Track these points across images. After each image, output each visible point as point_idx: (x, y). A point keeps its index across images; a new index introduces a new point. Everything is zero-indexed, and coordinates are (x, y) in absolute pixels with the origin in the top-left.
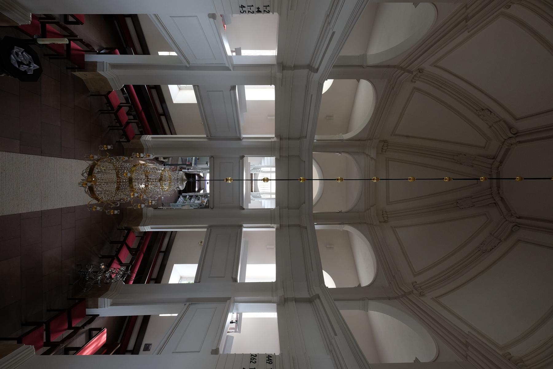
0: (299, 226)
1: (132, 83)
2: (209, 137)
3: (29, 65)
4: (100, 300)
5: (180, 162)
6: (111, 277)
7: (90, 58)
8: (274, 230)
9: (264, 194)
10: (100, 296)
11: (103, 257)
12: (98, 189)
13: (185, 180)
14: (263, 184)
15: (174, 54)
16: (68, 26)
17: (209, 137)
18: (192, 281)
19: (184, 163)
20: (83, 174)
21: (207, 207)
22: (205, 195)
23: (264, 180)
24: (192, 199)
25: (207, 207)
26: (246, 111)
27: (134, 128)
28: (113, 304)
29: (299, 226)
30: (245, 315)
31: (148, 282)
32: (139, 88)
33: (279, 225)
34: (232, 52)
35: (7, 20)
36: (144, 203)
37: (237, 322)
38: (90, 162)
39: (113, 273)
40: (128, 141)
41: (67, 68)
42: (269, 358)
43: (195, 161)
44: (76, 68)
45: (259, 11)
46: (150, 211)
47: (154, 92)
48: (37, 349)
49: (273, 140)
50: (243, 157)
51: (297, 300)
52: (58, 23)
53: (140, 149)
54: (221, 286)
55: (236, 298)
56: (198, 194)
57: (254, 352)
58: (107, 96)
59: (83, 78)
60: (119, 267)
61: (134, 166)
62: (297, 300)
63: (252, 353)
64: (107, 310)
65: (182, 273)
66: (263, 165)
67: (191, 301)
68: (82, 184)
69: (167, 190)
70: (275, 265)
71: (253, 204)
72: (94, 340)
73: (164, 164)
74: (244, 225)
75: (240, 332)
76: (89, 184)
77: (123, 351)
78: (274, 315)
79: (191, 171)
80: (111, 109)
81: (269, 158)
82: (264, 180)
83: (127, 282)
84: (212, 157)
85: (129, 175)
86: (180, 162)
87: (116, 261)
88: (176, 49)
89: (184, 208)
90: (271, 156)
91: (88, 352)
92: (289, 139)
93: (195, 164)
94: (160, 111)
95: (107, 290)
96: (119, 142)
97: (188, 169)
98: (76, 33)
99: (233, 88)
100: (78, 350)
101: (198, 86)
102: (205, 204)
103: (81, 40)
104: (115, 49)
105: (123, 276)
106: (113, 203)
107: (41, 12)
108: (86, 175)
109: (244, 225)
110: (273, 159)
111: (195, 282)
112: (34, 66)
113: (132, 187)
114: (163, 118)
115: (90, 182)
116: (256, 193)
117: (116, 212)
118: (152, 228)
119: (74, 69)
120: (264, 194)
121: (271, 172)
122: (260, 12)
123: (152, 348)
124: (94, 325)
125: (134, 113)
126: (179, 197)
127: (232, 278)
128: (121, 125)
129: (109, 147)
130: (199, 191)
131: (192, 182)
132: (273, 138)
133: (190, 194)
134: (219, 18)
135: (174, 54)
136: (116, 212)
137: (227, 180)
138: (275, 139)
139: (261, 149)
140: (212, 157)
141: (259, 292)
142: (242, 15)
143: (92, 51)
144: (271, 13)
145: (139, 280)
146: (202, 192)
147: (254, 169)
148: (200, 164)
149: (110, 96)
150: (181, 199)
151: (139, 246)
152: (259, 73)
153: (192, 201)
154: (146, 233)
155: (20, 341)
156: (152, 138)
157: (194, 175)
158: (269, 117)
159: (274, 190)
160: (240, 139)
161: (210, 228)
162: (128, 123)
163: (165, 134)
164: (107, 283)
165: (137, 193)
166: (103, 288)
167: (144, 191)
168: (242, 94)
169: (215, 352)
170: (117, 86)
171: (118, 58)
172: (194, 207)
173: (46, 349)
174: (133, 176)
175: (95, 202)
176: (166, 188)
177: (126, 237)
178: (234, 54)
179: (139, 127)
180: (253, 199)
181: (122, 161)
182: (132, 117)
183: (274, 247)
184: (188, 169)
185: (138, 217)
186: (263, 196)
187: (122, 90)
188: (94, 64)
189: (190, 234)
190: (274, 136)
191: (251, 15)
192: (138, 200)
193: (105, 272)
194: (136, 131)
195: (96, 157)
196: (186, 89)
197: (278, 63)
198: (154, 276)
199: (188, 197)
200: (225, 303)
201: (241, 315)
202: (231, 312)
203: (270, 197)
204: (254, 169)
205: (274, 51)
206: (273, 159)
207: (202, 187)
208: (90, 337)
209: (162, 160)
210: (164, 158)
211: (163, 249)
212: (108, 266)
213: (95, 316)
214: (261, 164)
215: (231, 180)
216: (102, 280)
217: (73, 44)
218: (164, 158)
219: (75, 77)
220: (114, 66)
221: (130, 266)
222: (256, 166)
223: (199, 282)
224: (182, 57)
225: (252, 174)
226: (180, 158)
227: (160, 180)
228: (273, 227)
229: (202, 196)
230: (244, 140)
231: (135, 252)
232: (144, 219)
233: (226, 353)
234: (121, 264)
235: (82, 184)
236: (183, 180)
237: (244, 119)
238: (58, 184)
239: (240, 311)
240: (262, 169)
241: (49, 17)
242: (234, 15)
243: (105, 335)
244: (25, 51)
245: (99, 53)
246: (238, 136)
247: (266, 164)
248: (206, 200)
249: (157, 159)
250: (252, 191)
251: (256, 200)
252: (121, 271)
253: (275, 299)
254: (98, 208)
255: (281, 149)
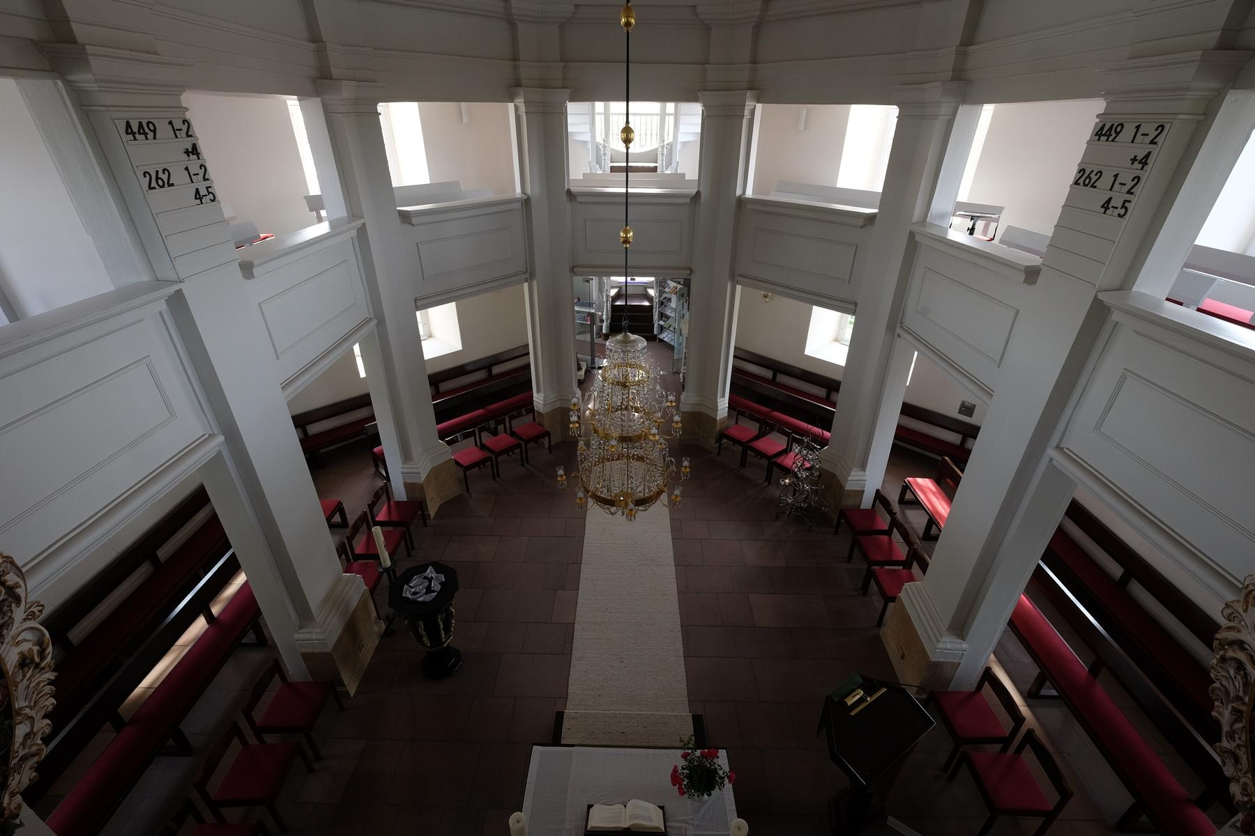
0: (758, 27)
1: (434, 428)
2: (527, 275)
3: (430, 580)
4: (849, 487)
5: (587, 337)
6: (807, 469)
7: (399, 492)
8: (759, 107)
9: (662, 135)
10: (841, 487)
11: (768, 478)
12: (641, 492)
13: (626, 336)
14: (639, 137)
15: (357, 348)
16: (351, 523)
17: (527, 275)
18: (851, 319)
19: (588, 328)
20: (612, 514)
21: (687, 283)
22: (661, 285)
23: (627, 141)
24: (668, 313)
25: (687, 283)
26: (458, 182)
27: (521, 423)
28: (863, 467)
29: (758, 27)
30: (963, 196)
31: (834, 405)
32: (441, 414)
33: (749, 94)
34: (320, 219)
35: (363, 601)
36: (672, 416)
37: (976, 214)
38: (591, 502)
39: (803, 465)
40: (547, 434)
41: (425, 525)
42: (1105, 132)
43: (583, 305)
44: (423, 514)
45: (194, 151)
46: (689, 399)
47: (444, 386)
48: (911, 579)
49: (523, 109)
50: (569, 192)
51: (969, 39)
52: (350, 539)
53: (563, 413)
54: (879, 252)
55: (915, 220)
56: (656, 300)
57: (1071, 174)
58: (467, 468)
59: (438, 503)
60: (792, 454)
61: (596, 431)
62: (969, 39)
63: (1071, 181)
64: (871, 477)
65: (827, 338)
66: (587, 138)
67: (896, 323)
68: (631, 516)
69: (647, 372)
70: (853, 106)
71: (688, 165)
72: (921, 496)
73: (589, 372)
74: (739, 192)
75: (999, 210)
76: (631, 506)
77: (962, 455)
78: (988, 111)
79: (605, 314)
80: (489, 461)
81: (570, 119)
82: (627, 141)
83: (823, 442)
84: (572, 270)
85: (614, 442)
86: (587, 337)
87: (780, 460)
88: (344, 347)
89: (685, 331)
90: (563, 114)
91: (941, 507)
92: (515, 59)
93: (590, 305)
94: (481, 375)
95: (833, 476)
96: (550, 447)
97: (602, 321)
98: (359, 513)
99: (405, 217)
100: (932, 521)
101: (416, 300)
102: (679, 286)
103: (371, 506)
104: (374, 453)
105: (813, 449)
106: (668, 467)
107: (337, 564)
108: (613, 509)
109: (739, 192)
110: (573, 108)
111: (853, 313)
112: (430, 572)
113: (639, 437)
114: (497, 370)
115: (627, 504)
116: (659, 157)
117: (686, 463)
118: (723, 396)
119: (425, 517)
120: (662, 135)
121: (607, 114)
122: (194, 146)
123: (970, 399)
124: (893, 496)
125: (492, 424)
126: (661, 340)
127: (862, 227)
128: (519, 446)
129: (561, 472)
130: (650, 299)
131: (631, 319)
132: (516, 108)
133: (656, 317)
134: (246, 253)
135: (357, 348)
136: (686, 463)
137: (626, 241)
138: (520, 101)
139: (548, 142)
140: (573, 270)
141: (913, 161)
142: (219, 197)
143: (386, 490)
144: (188, 116)
145: (826, 421)
146: (652, 292)
147: (598, 162)
148: (590, 294)
149: (465, 461)
150: (666, 336)
151: (756, 420)
152: (356, 150)
153: (672, 315)
154: (731, 407)
155: (890, 599)
156: (538, 391)
157: (614, 308)
158: (465, 121)
159: (654, 107)
160: (526, 202)
161: (734, 277)
162: (513, 434)
163: (529, 366)
164: (820, 476)
165: (650, 428)
166: (828, 482)
167: (647, 414)
168: (415, 194)
169: (1032, 274)
170: (444, 452)
171: (389, 446)
172: (686, 310)
173: (915, 566)
174: (616, 435)
175: (664, 497)
176: (640, 375)
177: (735, 441)
178: (323, 213)
179: (520, 415)
180: (674, 165)
181: (589, 451)
182: (501, 427)
183: (804, 109)
184: (602, 321)
185: (699, 420)
186: (669, 139)
187: (449, 443)
188: (409, 487)
189: (744, 320)
190: (511, 106)
191: (211, 173)
192: (665, 429)
193: (797, 477)
194: (527, 419)
195: (580, 494)
196: (427, 323)
197: (317, 93)
198: (821, 392)
199: (662, 323)
200: (317, 82)
201: (960, 206)
202: (946, 231)
203: (672, 118)
204: (598, 162)
205: (289, 102)
206: (573, 108)
207: (640, 291)
208: (916, 503)
209: (582, 372)
210: (579, 369)
211: (768, 374)
212: (787, 471)
213: (879, 496)
214: (585, 142)
215: (626, 232)
216: (812, 483)
217: (381, 517)
218: (579, 369)
219: (441, 513)
220: (406, 456)
221: (794, 436)
222: (591, 157)
223: (856, 304)
224: (359, 334)
225: (613, 169)
226: (578, 337)
227: (624, 385)
228: (753, 112)
229: (661, 293)
230: (529, 191)
231: (767, 426)
232: (704, 410)
233: (1044, 250)
234: (786, 452)
235: (631, 516)
236: (626, 342)
237: (478, 191)
238: (630, 580)
239: (950, 208)
240: (599, 138)
241: (342, 550)
242: (227, 215)
243: (920, 480)
244: (408, 582)
245: (388, 478)
246: (519, 205)
247: (587, 128)
248: (672, 284)
249: (581, 383)
250: (654, 169)
251: (677, 157)
252: (800, 451)
253: (945, 110)
254: (677, 492)
255: (544, 85)
